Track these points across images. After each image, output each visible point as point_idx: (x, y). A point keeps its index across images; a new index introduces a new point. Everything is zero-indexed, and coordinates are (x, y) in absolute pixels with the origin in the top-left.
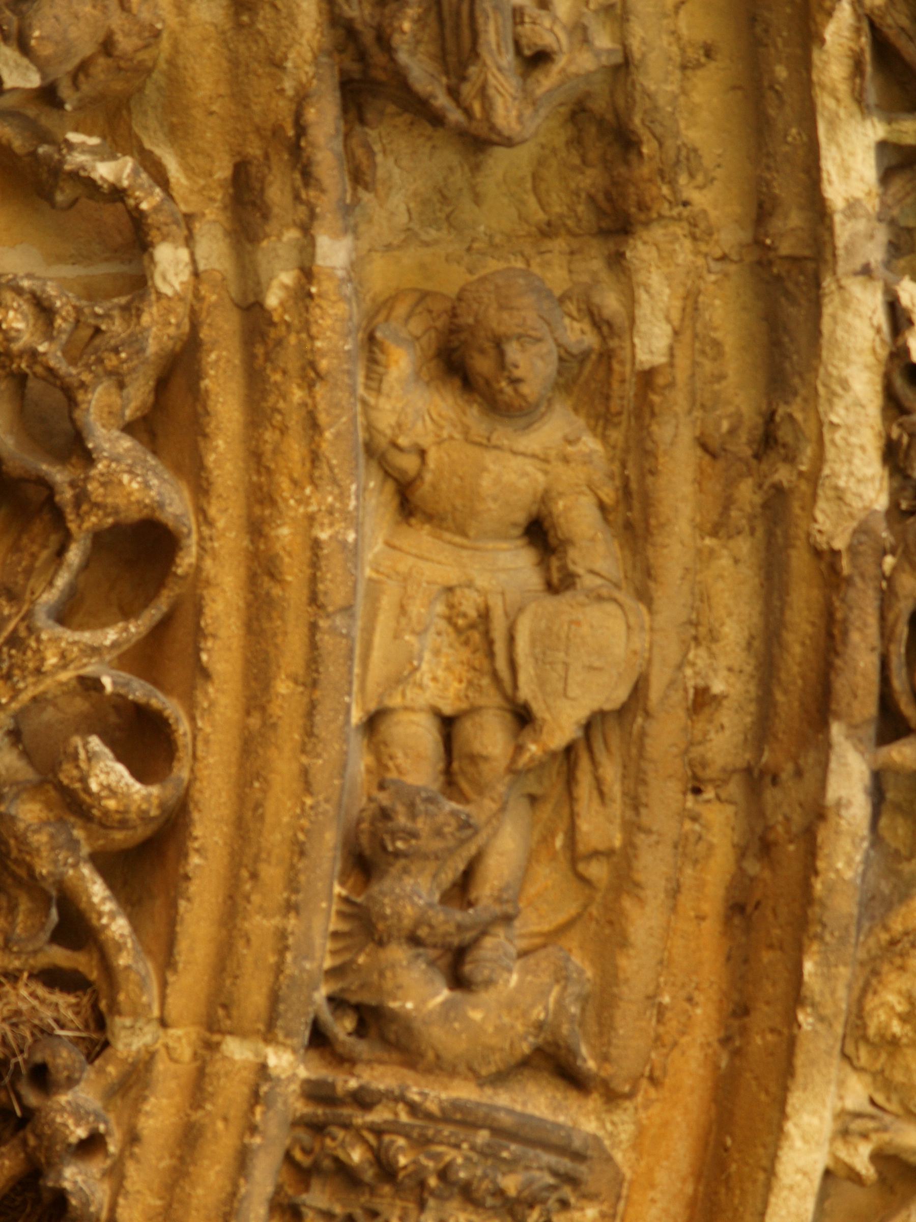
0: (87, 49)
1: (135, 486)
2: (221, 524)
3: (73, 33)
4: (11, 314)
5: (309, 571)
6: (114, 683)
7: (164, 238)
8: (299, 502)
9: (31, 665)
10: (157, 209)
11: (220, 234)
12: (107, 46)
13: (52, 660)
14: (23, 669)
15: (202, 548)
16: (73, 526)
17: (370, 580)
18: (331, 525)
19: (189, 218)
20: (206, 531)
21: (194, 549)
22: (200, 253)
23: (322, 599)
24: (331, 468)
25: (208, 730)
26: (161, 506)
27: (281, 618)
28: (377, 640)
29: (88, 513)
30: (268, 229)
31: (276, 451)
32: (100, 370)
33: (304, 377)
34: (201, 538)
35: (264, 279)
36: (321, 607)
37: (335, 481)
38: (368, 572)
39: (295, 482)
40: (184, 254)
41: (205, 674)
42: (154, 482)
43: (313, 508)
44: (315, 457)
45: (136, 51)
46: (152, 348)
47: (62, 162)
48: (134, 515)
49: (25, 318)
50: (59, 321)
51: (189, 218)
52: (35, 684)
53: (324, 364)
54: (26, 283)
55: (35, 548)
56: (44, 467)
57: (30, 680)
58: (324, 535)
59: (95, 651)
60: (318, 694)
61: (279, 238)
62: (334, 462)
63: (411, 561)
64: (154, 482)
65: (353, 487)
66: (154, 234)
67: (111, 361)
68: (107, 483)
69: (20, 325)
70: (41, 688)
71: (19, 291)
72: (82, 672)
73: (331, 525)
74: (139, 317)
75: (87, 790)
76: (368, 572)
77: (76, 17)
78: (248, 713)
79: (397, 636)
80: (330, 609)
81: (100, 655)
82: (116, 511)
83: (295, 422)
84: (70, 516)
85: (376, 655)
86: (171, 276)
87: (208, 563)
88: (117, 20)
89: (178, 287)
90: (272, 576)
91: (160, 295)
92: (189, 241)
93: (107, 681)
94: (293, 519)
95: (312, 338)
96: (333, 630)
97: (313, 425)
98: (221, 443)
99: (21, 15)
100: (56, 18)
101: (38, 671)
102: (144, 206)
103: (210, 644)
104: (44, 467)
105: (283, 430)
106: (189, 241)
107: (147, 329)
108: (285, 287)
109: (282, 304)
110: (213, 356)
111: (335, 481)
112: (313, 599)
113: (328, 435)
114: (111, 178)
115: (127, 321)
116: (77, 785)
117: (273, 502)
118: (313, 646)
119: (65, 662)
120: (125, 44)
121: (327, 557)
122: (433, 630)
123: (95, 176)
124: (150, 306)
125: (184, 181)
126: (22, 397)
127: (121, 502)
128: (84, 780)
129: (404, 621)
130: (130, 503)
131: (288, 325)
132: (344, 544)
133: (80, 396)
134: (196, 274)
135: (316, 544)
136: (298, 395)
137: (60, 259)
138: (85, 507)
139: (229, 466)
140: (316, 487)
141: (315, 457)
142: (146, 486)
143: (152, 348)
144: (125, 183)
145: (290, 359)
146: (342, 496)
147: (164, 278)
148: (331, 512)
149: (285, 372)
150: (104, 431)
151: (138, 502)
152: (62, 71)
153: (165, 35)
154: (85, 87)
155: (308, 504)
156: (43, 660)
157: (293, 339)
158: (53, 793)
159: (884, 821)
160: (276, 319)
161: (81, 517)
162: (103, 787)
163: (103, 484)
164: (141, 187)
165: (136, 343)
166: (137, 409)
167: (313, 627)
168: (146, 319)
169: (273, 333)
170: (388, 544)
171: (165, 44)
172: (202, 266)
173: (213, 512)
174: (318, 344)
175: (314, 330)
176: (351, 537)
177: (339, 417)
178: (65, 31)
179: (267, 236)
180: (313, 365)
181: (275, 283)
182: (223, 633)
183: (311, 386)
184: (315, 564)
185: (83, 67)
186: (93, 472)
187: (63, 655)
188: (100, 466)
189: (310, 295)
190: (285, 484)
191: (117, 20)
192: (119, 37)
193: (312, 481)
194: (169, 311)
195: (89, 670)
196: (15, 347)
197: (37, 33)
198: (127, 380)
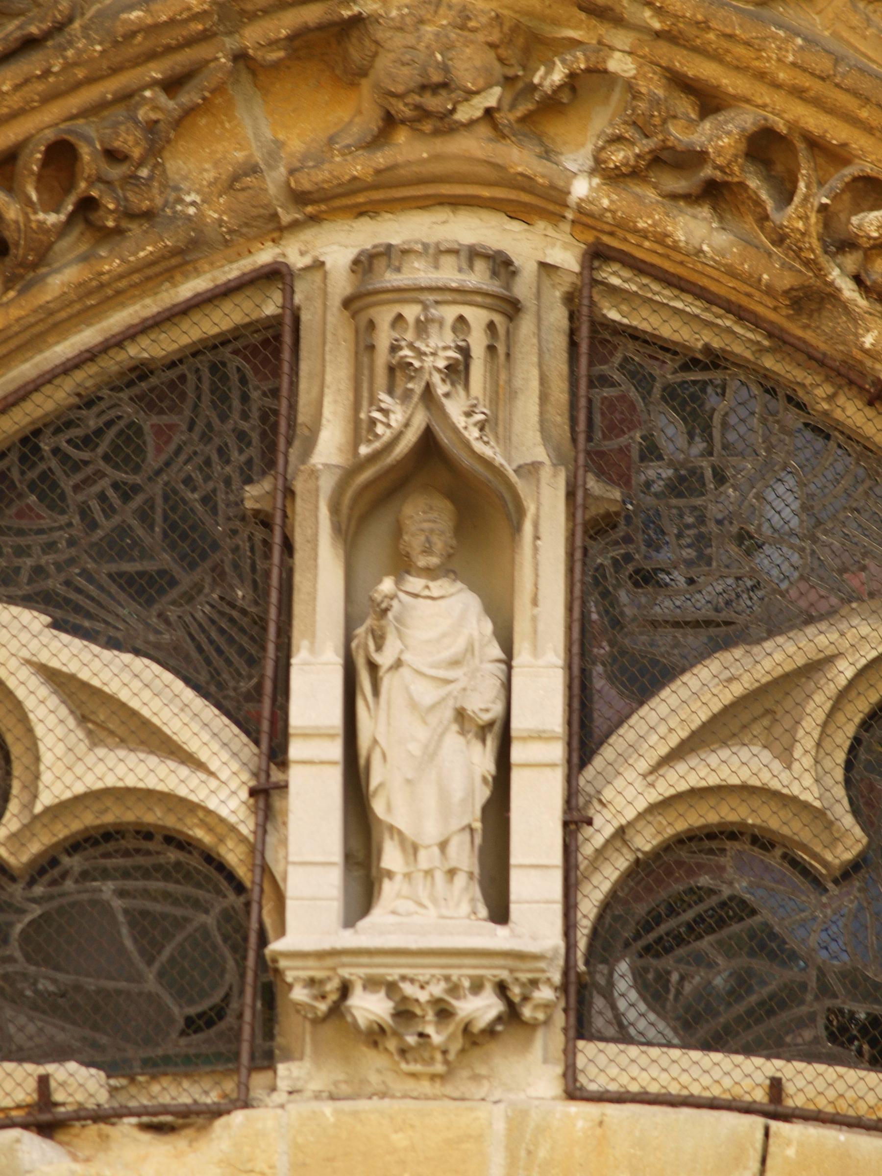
0: (491, 55)
1: (726, 140)
2: (768, 100)
3: (478, 63)
4: (613, 158)
5: (807, 74)
6: (827, 197)
7: (605, 62)
8: (769, 61)
9: (798, 236)
10: (587, 59)
11: (614, 31)
12: (492, 46)
13: (800, 225)
14: (799, 240)
15: (777, 115)
16: (736, 180)
17: (831, 34)
18: (787, 51)
19: (600, 42)
20: (769, 109)
21: (777, 118)
22: (620, 47)
23: (824, 75)
24: (757, 38)
25: (874, 157)
26: (744, 130)
27: (826, 98)
28: (863, 49)
29: (731, 170)
30: (618, 11)
31: (738, 59)
32: (659, 128)
33: (703, 29)
34: (772, 113)
35: (643, 24)
36: (828, 76)
37: (764, 39)
38: (827, 33)
39: (757, 59)
40: (617, 55)
41: (844, 145)
42: (730, 127)
43: (774, 56)
44: (748, 44)
45: (501, 31)
46: (660, 93)
47: (546, 94)
48: (743, 147)
49: (618, 150)
50: (627, 135)
51: (600, 42)
52: (810, 237)
53: (700, 17)
54: (600, 143)
55: (745, 195)
56: (702, 175)
57: (806, 239)
58: (791, 58)
59: (806, 199)
60: (874, 100)
61: (624, 7)
62: (754, 34)
63: (830, 9)
64: (730, 127)
65: (773, 29)
66: (600, 67)
67: (657, 121)
68: (719, 152)
69: (621, 155)
70: (814, 234)
71: (603, 148)
72: (815, 208)
73: (787, 51)
74: (641, 93)
75: (875, 239)
76: (827, 33)
77: (470, 58)
78: (873, 135)
79: (865, 38)
80: (831, 72)
81: (810, 195)
82: (736, 156)
83: (725, 44)
84: (729, 179)
85: (870, 53)
86: (626, 67)
87: (786, 116)
88: (481, 37)
89: (633, 66)
90: (803, 91)
91: (634, 78)
92: (612, 48)
93: (825, 200)
94: (777, 68)
95: (684, 17)
96: (844, 76)
97: (730, 37)
98: (725, 81)
99: (459, 88)
100: (467, 70)
101: (803, 234)
102: (583, 66)
103: (828, 135)
104: (702, 175)
105: (728, 51)
106: (612, 48)
107: (650, 90)
108: (652, 17)
109: (660, 22)
110: (677, 64)
111: (764, 39)
112: (823, 79)
113: (738, 32)
114: (562, 75)
115: (641, 99)
116: (872, 242)
117: (765, 73)
118: (847, 90)
119: (805, 218)
120: (495, 37)
121: (803, 61)
122: (871, 15)
123: (558, 83)
124: (637, 85)
125: (581, 33)
126: (665, 163)
127: (732, 151)
128: (870, 238)
129: (858, 31)
130: (734, 147)
131: (673, 24)
132: (801, 48)
133: (670, 144)
134: (630, 53)
135: (794, 64)
136: (711, 36)
137: (607, 98)
138: (727, 170)
139: (739, 82)
140: (764, 50)
141: (748, 44)
142: (729, 133)
143: (660, 93)
144: (567, 71)
145: (691, 32)
146: (774, 37)
147: (625, 71)
148: (780, 48)
149: (697, 37)
150: (696, 135)
151: (736, 142)
152: (498, 70)
153: (500, 11)
154: (513, 61)
155: (771, 58)
156: (798, 230)
157: (681, 25)
158: (874, 252)
159: (497, 709)
160: (667, 28)
161: (732, 174)
162: (877, 230)
163: (719, 155)
164: (573, 62)
165: (655, 102)
166: (694, 109)
167: (837, 85)
168: (644, 90)
169: (675, 33)
170: (819, 13)
171: (505, 12)
172: (627, 49)
173: (759, 102)
174: (688, 15)
175: (680, 14)
176: (799, 41)
177: (732, 21)
178: (475, 67)
179: (622, 13)
180: (698, 23)
181: (649, 20)
182: (826, 126)
183: (709, 28)
184: (805, 70)
185: (500, 60)
186: (712, 156)
187: (800, 218)
188: (710, 150)
189: (660, 8)
190: (756, 63)
191: (481, 37)
192: (490, 39)
193: (759, 50)
194: (645, 76)
195: (816, 204)
196: (632, 162)
197: (469, 85)
198: (672, 113)
